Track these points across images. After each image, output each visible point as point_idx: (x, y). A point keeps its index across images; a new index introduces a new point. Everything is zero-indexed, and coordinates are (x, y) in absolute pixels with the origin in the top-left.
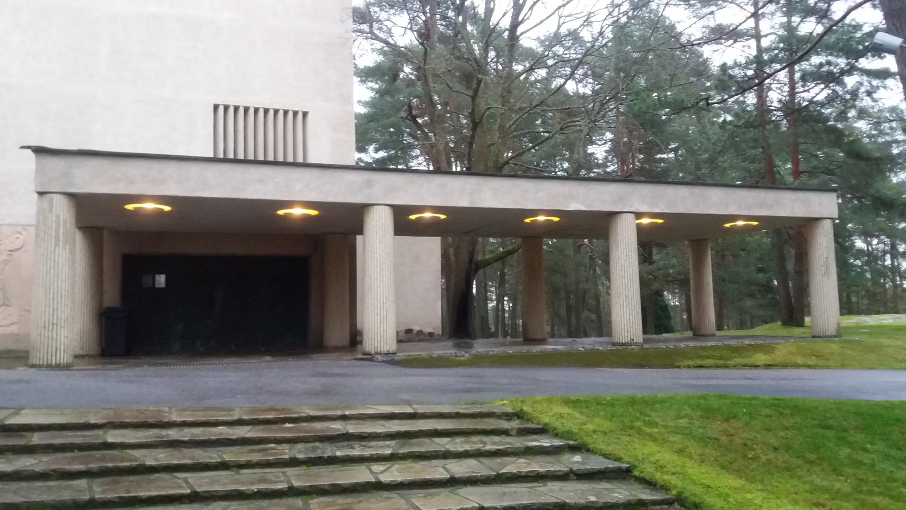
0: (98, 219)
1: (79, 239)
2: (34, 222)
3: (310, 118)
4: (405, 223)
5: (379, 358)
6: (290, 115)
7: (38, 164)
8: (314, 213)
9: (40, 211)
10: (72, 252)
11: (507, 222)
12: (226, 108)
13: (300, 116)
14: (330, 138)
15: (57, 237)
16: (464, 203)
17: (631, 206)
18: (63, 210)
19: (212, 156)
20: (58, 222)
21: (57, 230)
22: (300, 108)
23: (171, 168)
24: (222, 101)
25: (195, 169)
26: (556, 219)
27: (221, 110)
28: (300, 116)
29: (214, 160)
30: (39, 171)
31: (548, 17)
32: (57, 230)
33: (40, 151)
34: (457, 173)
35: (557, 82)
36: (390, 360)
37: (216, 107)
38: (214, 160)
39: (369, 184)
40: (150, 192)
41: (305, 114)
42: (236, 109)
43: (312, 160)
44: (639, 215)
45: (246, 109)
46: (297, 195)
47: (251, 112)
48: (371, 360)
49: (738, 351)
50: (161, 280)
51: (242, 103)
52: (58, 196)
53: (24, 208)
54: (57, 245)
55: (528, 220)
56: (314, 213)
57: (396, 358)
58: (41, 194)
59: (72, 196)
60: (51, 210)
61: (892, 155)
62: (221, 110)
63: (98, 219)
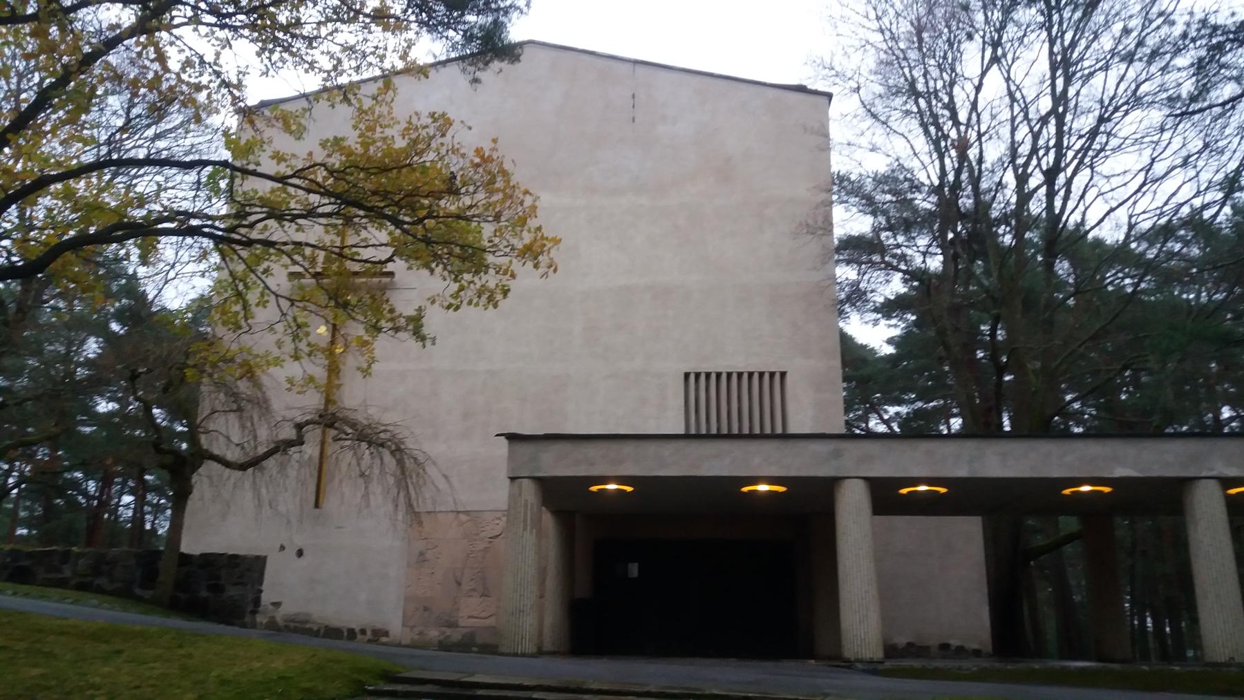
0: (565, 500)
1: (548, 519)
2: (505, 507)
3: (788, 378)
4: (887, 497)
5: (859, 666)
6: (767, 377)
7: (510, 451)
9: (512, 498)
10: (540, 534)
11: (1042, 495)
13: (777, 377)
15: (525, 521)
16: (962, 472)
17: (1212, 470)
18: (529, 492)
19: (682, 432)
20: (526, 506)
21: (525, 513)
23: (628, 448)
24: (692, 367)
25: (668, 448)
26: (1107, 490)
27: (692, 378)
28: (777, 377)
30: (511, 456)
31: (1179, 188)
32: (525, 513)
33: (512, 438)
34: (1078, 436)
36: (872, 668)
37: (687, 375)
38: (687, 436)
39: (837, 454)
40: (613, 476)
41: (783, 374)
43: (793, 429)
44: (1227, 482)
45: (719, 375)
46: (763, 471)
47: (724, 377)
48: (849, 667)
50: (634, 570)
51: (712, 367)
52: (1213, 481)
53: (498, 494)
54: (525, 529)
55: (1067, 492)
57: (880, 667)
58: (512, 479)
60: (520, 495)
61: (1128, 294)
62: (692, 378)
63: (565, 500)
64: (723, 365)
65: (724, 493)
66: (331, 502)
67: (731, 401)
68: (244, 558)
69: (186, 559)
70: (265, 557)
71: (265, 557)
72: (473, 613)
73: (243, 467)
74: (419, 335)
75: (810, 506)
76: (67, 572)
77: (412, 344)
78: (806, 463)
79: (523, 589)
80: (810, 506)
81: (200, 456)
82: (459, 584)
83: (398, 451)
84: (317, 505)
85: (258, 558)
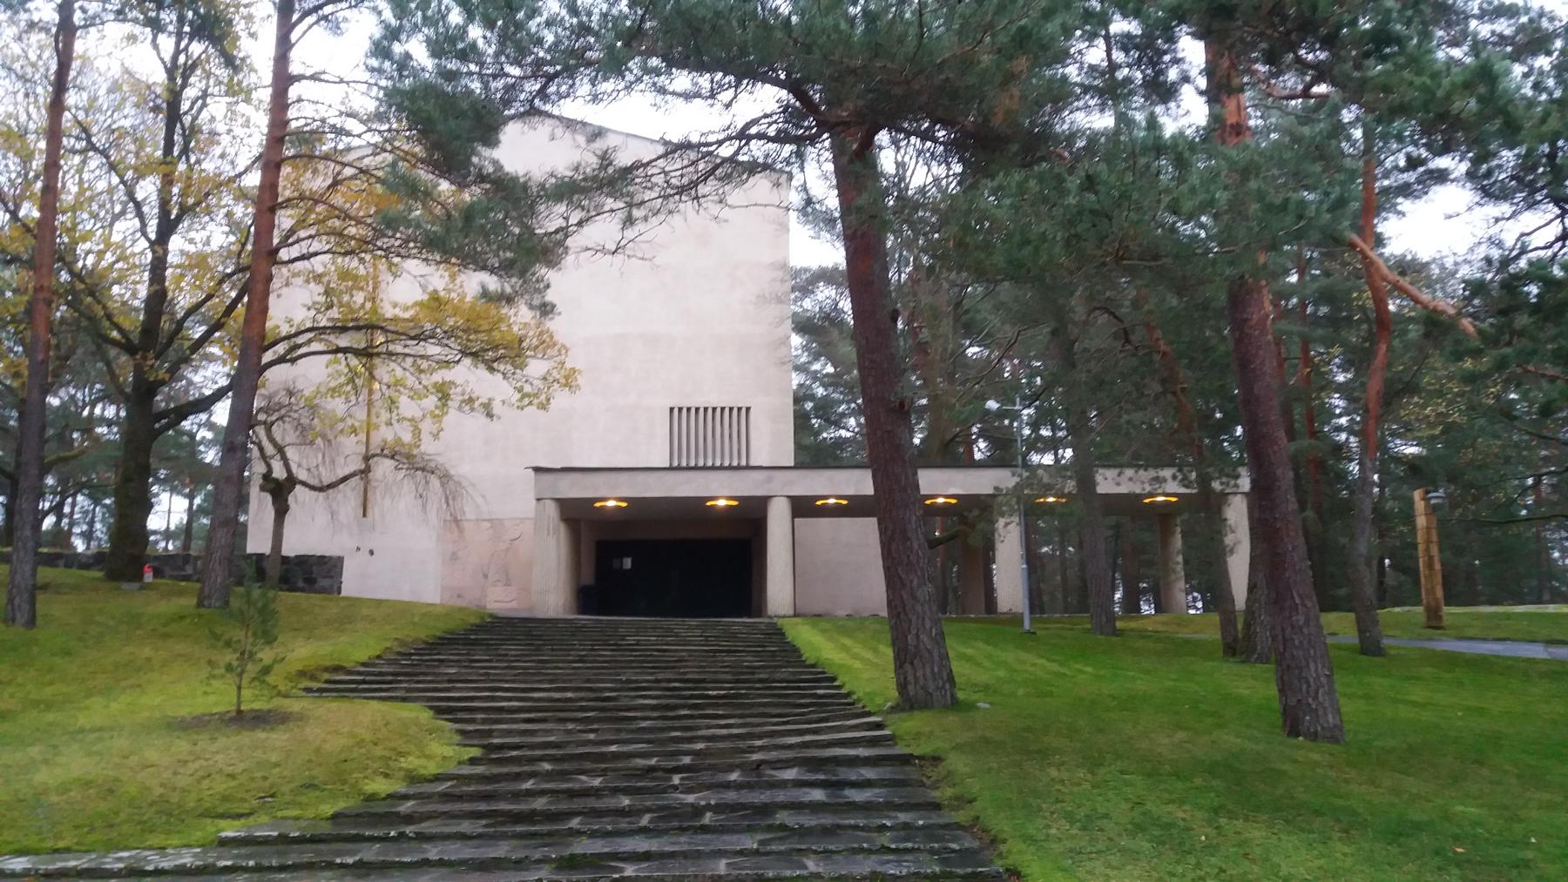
0: (578, 517)
8: (624, 504)
12: (680, 409)
14: (772, 440)
18: (552, 510)
22: (743, 405)
23: (624, 476)
24: (676, 403)
29: (671, 469)
33: (537, 470)
35: (1337, 402)
37: (672, 409)
38: (671, 469)
39: (769, 480)
41: (748, 409)
42: (689, 409)
43: (752, 463)
46: (722, 492)
49: (571, 773)
50: (628, 563)
51: (693, 404)
56: (624, 504)
59: (558, 500)
63: (578, 517)
64: (700, 402)
65: (696, 508)
66: (374, 511)
67: (705, 428)
68: (330, 558)
69: (286, 560)
70: (340, 560)
71: (340, 560)
72: (500, 600)
73: (321, 489)
74: (490, 415)
75: (752, 515)
76: (189, 570)
77: (484, 420)
78: (748, 486)
79: (543, 583)
80: (752, 515)
81: (292, 481)
82: (486, 576)
83: (445, 477)
84: (364, 515)
85: (322, 560)
